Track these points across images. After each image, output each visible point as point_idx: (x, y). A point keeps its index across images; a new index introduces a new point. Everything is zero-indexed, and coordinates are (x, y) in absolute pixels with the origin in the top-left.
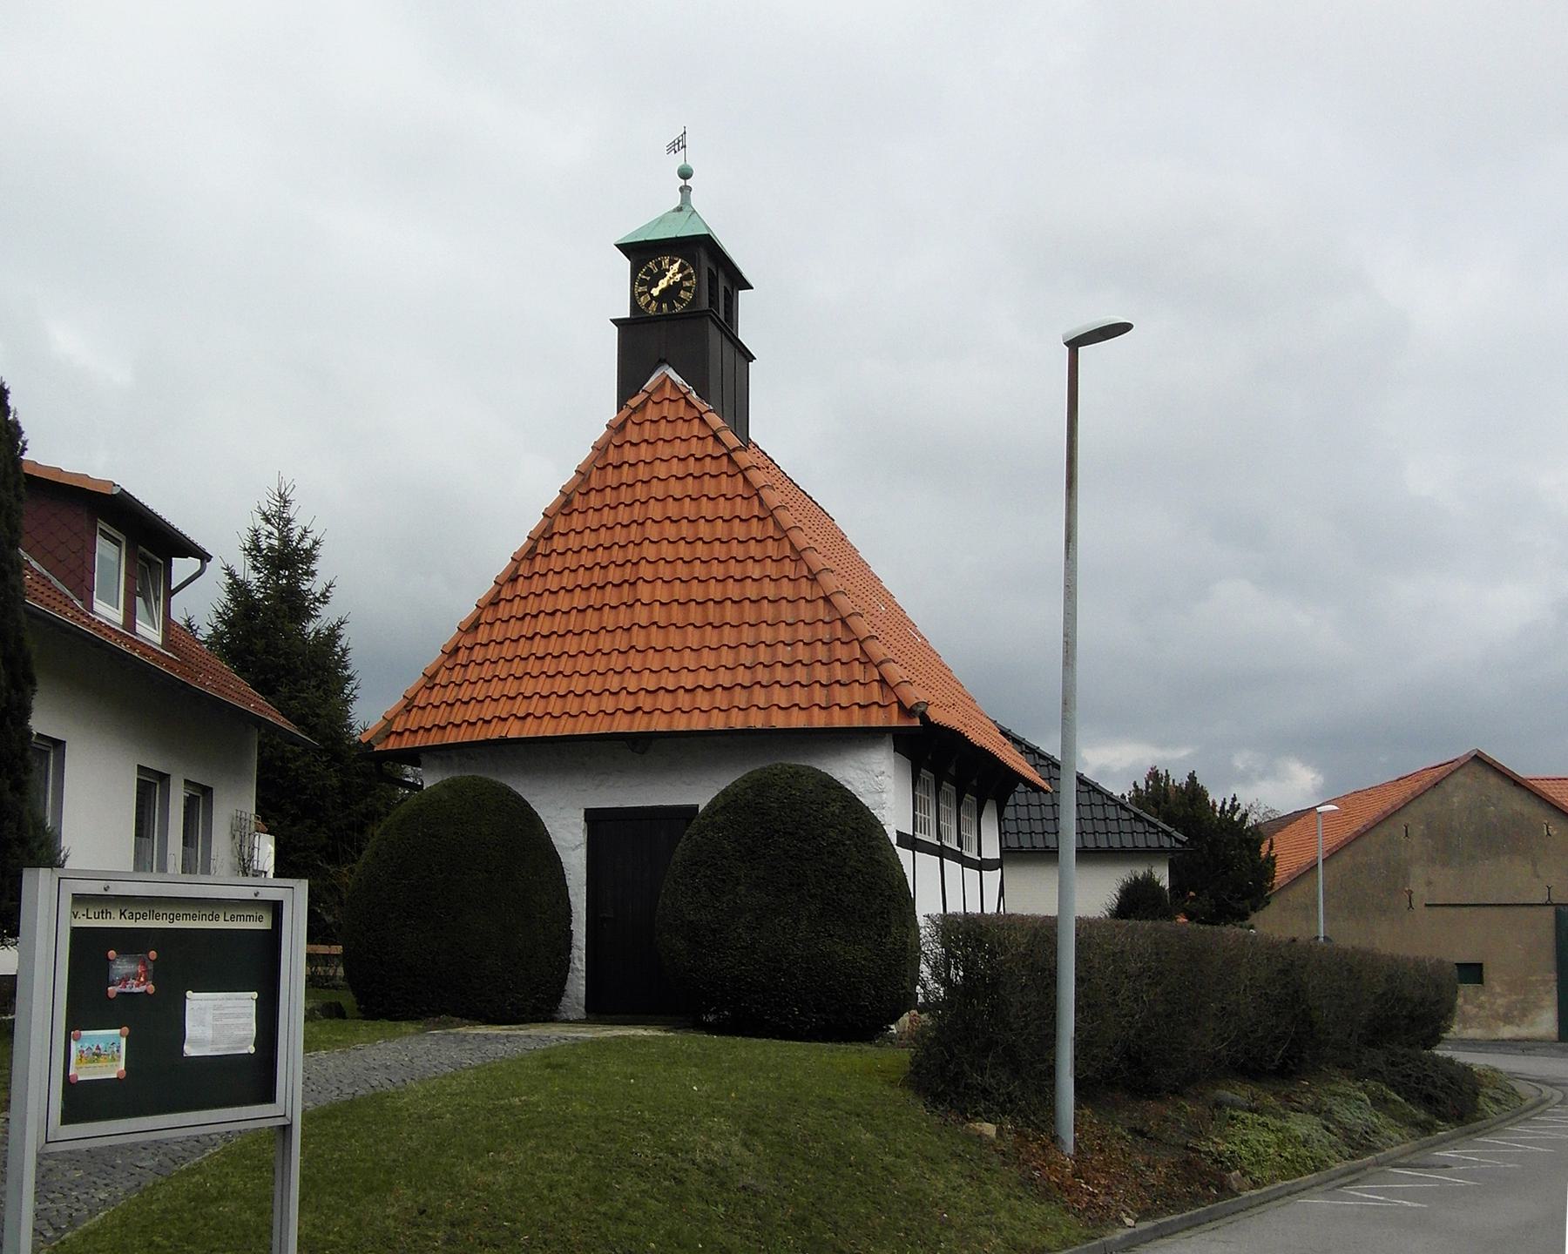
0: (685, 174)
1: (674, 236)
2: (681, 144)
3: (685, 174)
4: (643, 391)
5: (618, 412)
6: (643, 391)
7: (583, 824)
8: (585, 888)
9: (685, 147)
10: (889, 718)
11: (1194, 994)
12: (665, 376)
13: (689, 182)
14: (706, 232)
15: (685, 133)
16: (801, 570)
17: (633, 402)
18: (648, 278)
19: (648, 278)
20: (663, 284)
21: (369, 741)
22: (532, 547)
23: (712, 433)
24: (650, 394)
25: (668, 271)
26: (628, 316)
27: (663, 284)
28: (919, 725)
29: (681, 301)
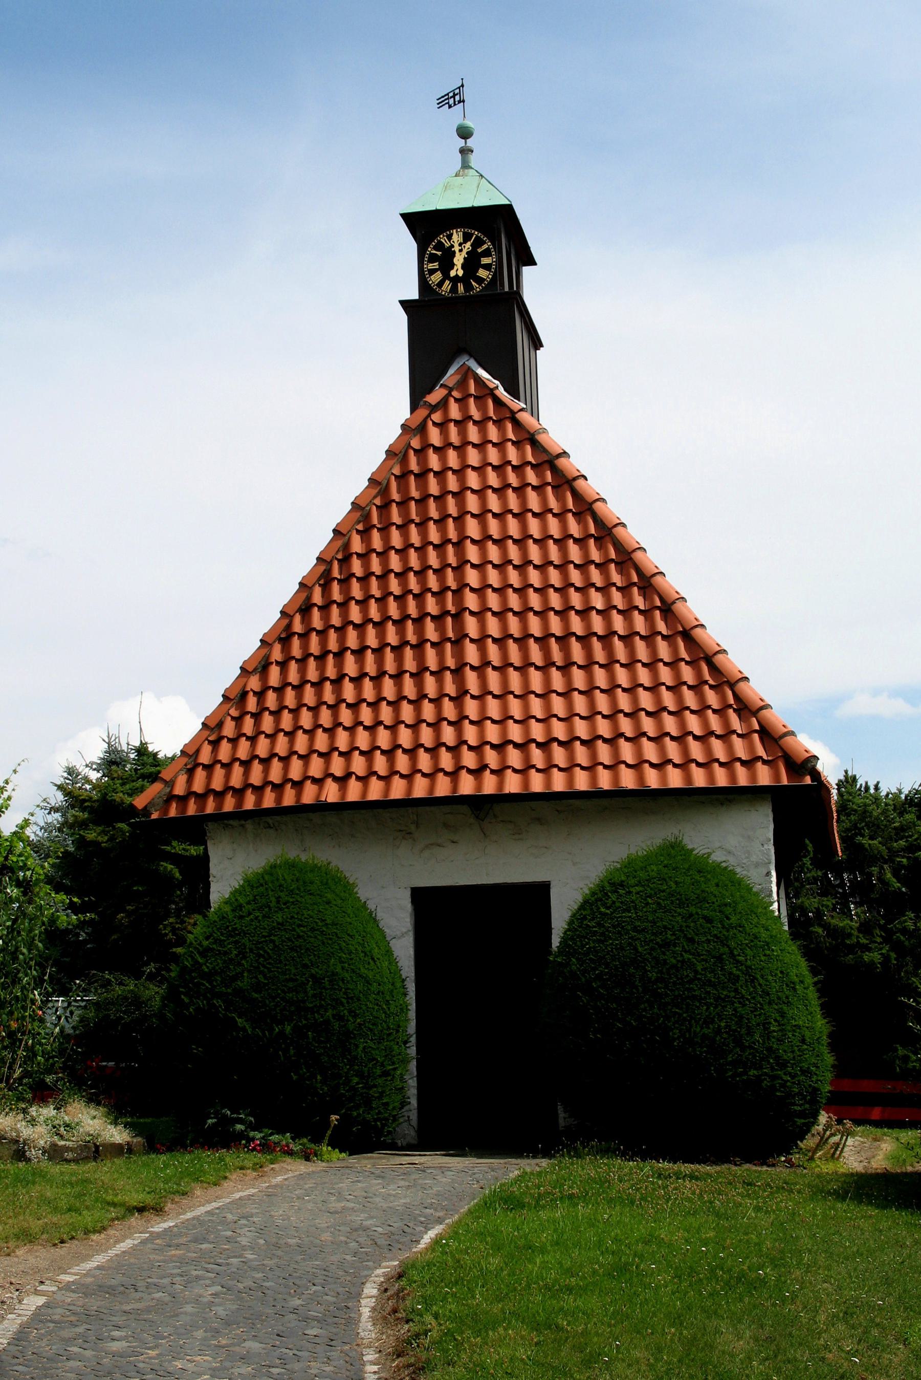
0: (464, 133)
1: (434, 209)
2: (457, 98)
3: (464, 133)
4: (442, 385)
5: (412, 412)
6: (442, 385)
7: (408, 906)
8: (414, 985)
9: (464, 101)
10: (777, 776)
11: (646, 1005)
12: (465, 368)
13: (470, 142)
14: (508, 203)
15: (462, 86)
16: (652, 601)
17: (434, 397)
18: (439, 253)
19: (439, 253)
20: (459, 260)
21: (146, 807)
22: (325, 570)
23: (528, 436)
24: (451, 390)
25: (452, 246)
26: (417, 297)
27: (459, 260)
28: (809, 782)
29: (480, 280)
